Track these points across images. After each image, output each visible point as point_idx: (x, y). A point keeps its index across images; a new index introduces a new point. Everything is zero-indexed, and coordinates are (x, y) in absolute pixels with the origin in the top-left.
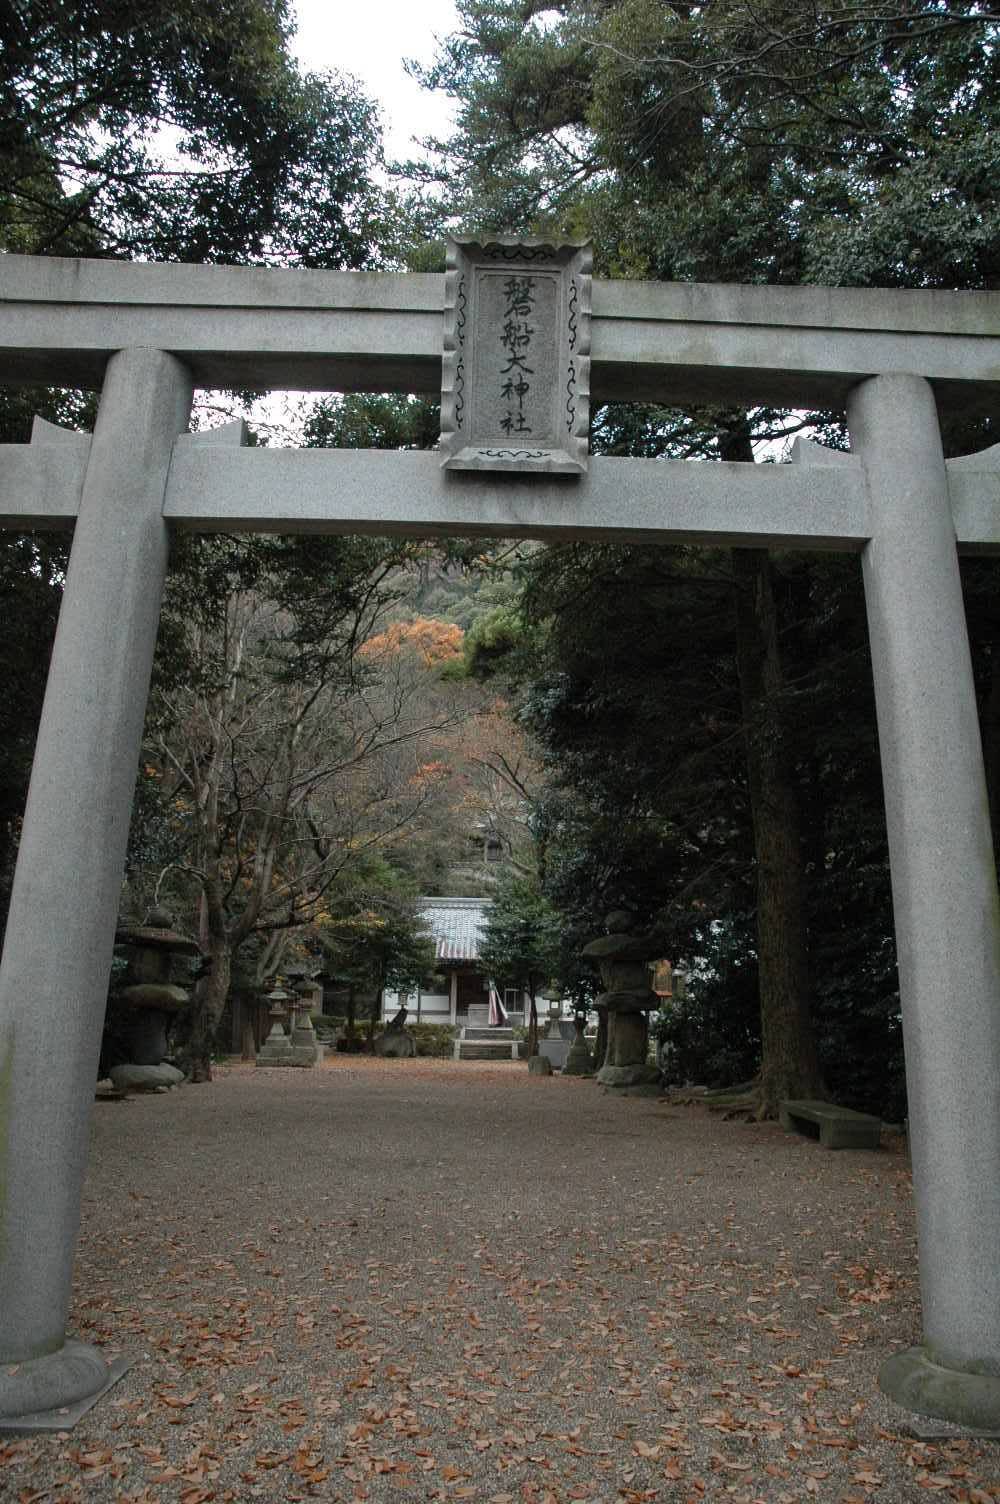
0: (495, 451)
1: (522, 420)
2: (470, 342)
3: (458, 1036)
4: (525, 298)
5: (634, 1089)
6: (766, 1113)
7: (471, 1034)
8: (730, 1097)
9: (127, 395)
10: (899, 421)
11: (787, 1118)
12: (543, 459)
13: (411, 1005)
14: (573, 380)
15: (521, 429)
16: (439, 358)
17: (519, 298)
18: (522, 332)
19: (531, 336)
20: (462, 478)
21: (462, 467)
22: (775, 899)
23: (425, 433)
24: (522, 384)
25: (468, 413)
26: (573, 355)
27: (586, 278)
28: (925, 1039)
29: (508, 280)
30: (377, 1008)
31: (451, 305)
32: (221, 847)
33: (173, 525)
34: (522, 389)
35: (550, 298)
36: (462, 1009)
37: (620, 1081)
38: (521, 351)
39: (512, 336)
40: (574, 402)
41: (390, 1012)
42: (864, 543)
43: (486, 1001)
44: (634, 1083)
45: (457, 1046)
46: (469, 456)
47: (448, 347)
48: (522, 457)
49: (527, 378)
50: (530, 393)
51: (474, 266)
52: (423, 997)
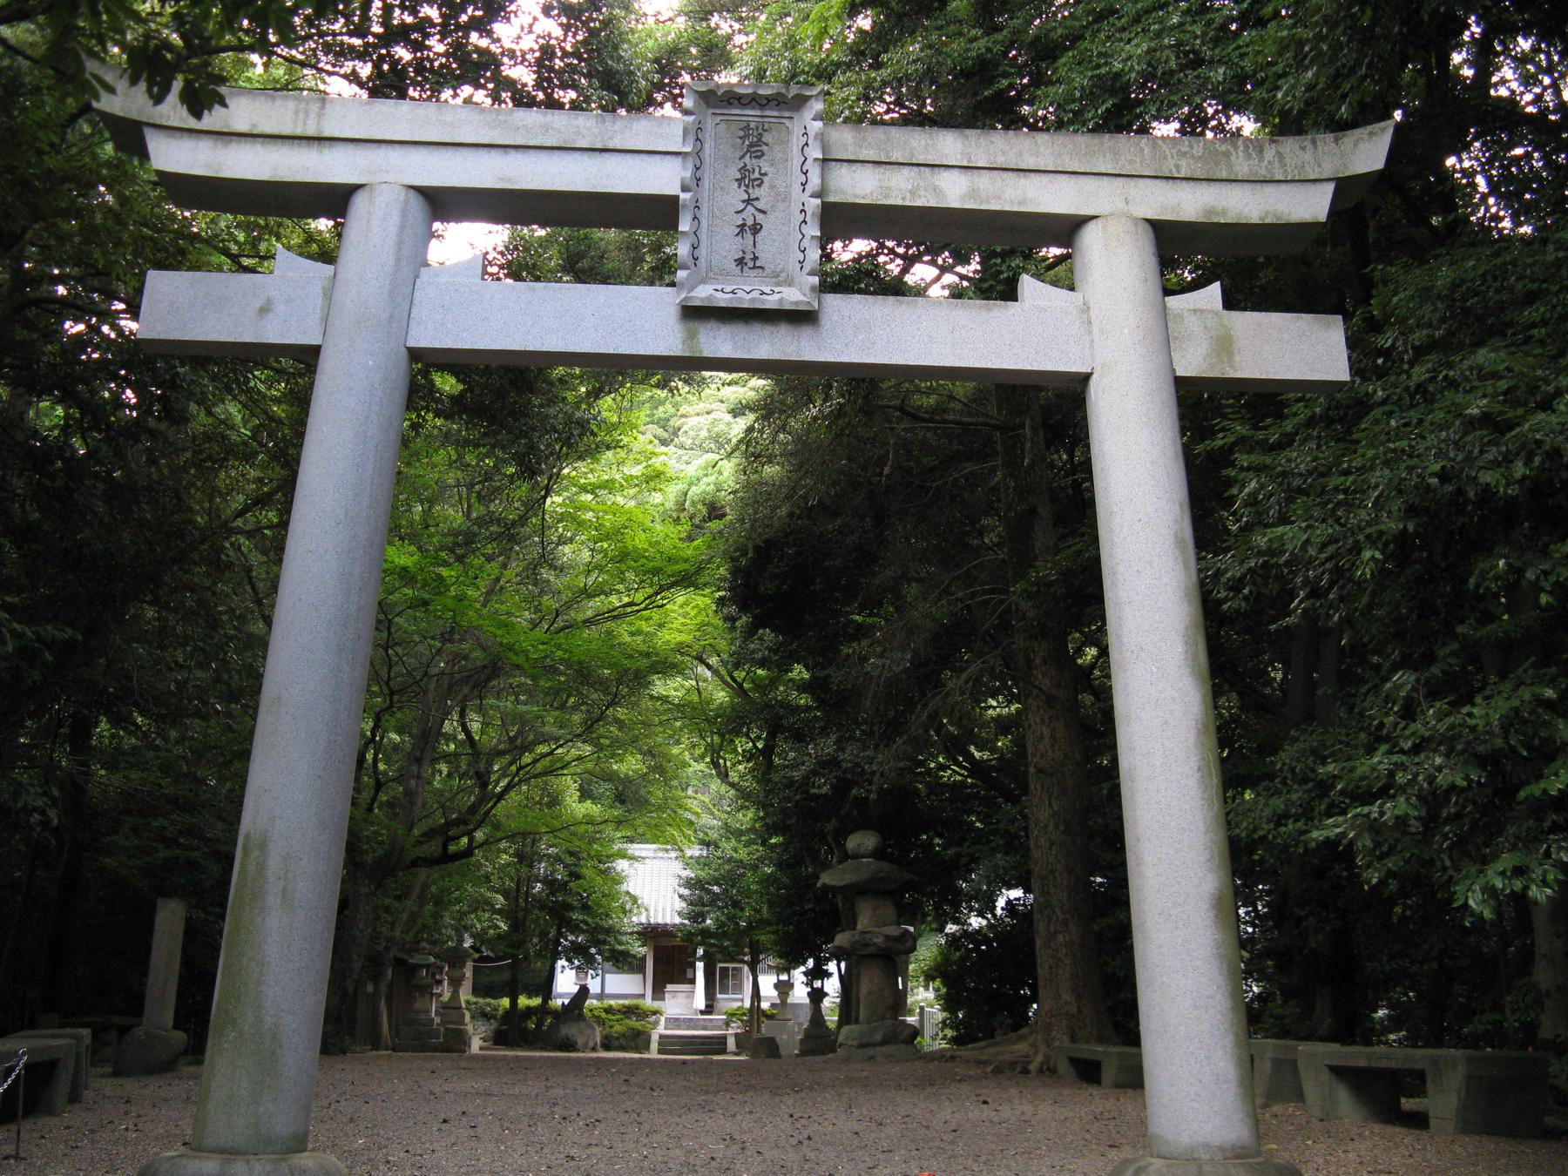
0: (729, 289)
1: (755, 258)
2: (706, 183)
3: (657, 1023)
4: (759, 142)
5: (887, 1049)
6: (1043, 1063)
7: (675, 1022)
8: (999, 1049)
9: (373, 228)
10: (1114, 264)
11: (1067, 1061)
12: (776, 297)
13: (594, 986)
14: (804, 222)
15: (755, 267)
16: (677, 197)
17: (754, 145)
18: (756, 175)
19: (766, 179)
20: (694, 314)
21: (699, 304)
22: (1050, 805)
23: (662, 272)
24: (755, 224)
25: (703, 252)
26: (805, 197)
27: (819, 124)
28: (1148, 859)
29: (743, 125)
30: (545, 987)
31: (688, 149)
32: (1269, 21)
33: (415, 354)
34: (756, 229)
35: (786, 143)
36: (658, 992)
37: (865, 1041)
38: (755, 193)
39: (747, 179)
40: (806, 243)
41: (561, 996)
42: (1085, 378)
43: (693, 981)
44: (883, 1043)
45: (655, 1038)
46: (704, 294)
47: (684, 189)
48: (755, 294)
49: (760, 218)
50: (763, 233)
51: (711, 111)
52: (607, 976)
